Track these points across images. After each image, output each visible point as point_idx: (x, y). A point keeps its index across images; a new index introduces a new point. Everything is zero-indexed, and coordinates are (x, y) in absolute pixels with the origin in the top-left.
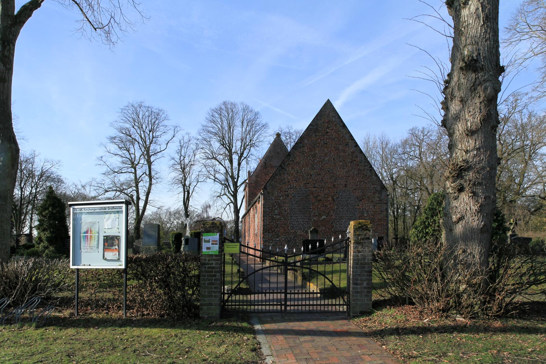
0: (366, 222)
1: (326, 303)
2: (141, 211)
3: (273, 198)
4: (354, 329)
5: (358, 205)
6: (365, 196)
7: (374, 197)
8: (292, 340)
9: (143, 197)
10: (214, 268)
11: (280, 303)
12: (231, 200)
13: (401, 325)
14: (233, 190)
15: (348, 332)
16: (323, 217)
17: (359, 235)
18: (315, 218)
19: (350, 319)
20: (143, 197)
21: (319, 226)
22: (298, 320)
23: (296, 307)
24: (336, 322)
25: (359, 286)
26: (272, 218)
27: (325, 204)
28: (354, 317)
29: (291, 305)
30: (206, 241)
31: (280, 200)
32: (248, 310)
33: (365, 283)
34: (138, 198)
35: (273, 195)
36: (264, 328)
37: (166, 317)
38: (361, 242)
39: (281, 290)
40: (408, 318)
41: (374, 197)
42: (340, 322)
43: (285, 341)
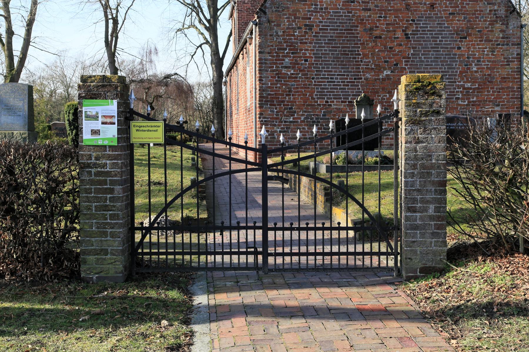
0: (431, 77)
1: (376, 249)
2: (16, 60)
3: (280, 33)
4: (401, 305)
5: (459, 48)
6: (473, 28)
7: (492, 31)
8: (262, 327)
9: (20, 30)
10: (108, 174)
11: (253, 250)
12: (205, 38)
13: (500, 297)
14: (208, 17)
15: (386, 310)
16: (385, 73)
17: (418, 105)
18: (368, 75)
19: (401, 283)
20: (20, 30)
21: (377, 92)
22: (289, 286)
23: (295, 259)
24: (370, 289)
25: (418, 214)
26: (279, 74)
27: (389, 45)
28: (409, 279)
29: (276, 255)
30: (88, 117)
31: (294, 35)
32: (193, 264)
33: (432, 207)
34: (10, 33)
35: (278, 25)
36: (212, 302)
37: (7, 278)
38: (422, 121)
39: (275, 224)
40: (518, 282)
41: (492, 31)
42: (378, 290)
43: (246, 328)
